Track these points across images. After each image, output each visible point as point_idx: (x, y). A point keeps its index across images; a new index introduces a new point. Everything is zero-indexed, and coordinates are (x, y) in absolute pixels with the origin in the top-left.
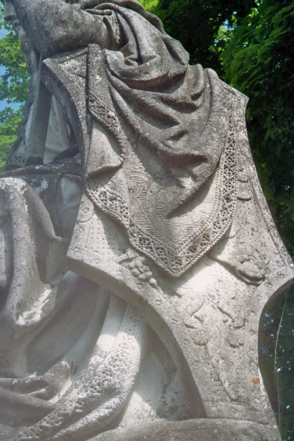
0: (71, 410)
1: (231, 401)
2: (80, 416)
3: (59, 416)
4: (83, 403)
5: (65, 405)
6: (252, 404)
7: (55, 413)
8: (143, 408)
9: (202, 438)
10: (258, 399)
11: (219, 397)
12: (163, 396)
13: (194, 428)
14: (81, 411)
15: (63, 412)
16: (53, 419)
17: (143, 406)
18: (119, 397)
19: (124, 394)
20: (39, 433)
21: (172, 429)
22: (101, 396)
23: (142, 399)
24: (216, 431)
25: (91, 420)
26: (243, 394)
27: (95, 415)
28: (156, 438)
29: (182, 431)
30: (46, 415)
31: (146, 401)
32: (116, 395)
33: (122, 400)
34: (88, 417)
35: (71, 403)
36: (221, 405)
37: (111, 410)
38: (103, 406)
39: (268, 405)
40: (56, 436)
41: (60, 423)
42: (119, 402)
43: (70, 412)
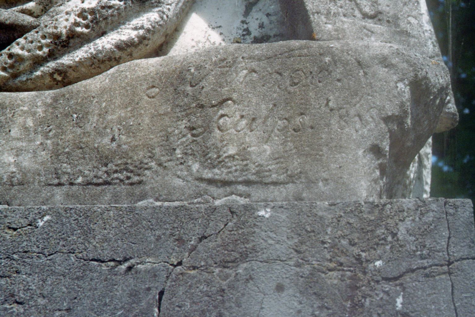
0: (66, 27)
1: (364, 18)
2: (85, 39)
3: (44, 37)
4: (89, 17)
5: (57, 20)
6: (403, 25)
7: (37, 32)
8: (208, 39)
9: (300, 72)
10: (415, 18)
11: (340, 10)
12: (244, 19)
13: (286, 54)
14: (85, 30)
15: (50, 30)
16: (32, 42)
17: (207, 35)
18: (160, 11)
19: (168, 7)
20: (6, 66)
21: (245, 55)
22: (125, 8)
23: (206, 25)
24: (327, 59)
25: (103, 47)
26: (388, 8)
27: (112, 39)
28: (212, 70)
29: (263, 58)
30: (20, 37)
31: (213, 28)
32: (153, 7)
33: (165, 17)
34: (98, 41)
35: (66, 17)
36: (342, 21)
37: (141, 32)
38: (129, 24)
39: (434, 46)
40: (38, 73)
41: (46, 50)
42: (158, 19)
43: (64, 31)
